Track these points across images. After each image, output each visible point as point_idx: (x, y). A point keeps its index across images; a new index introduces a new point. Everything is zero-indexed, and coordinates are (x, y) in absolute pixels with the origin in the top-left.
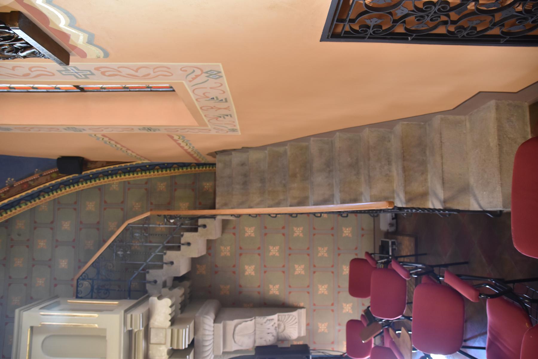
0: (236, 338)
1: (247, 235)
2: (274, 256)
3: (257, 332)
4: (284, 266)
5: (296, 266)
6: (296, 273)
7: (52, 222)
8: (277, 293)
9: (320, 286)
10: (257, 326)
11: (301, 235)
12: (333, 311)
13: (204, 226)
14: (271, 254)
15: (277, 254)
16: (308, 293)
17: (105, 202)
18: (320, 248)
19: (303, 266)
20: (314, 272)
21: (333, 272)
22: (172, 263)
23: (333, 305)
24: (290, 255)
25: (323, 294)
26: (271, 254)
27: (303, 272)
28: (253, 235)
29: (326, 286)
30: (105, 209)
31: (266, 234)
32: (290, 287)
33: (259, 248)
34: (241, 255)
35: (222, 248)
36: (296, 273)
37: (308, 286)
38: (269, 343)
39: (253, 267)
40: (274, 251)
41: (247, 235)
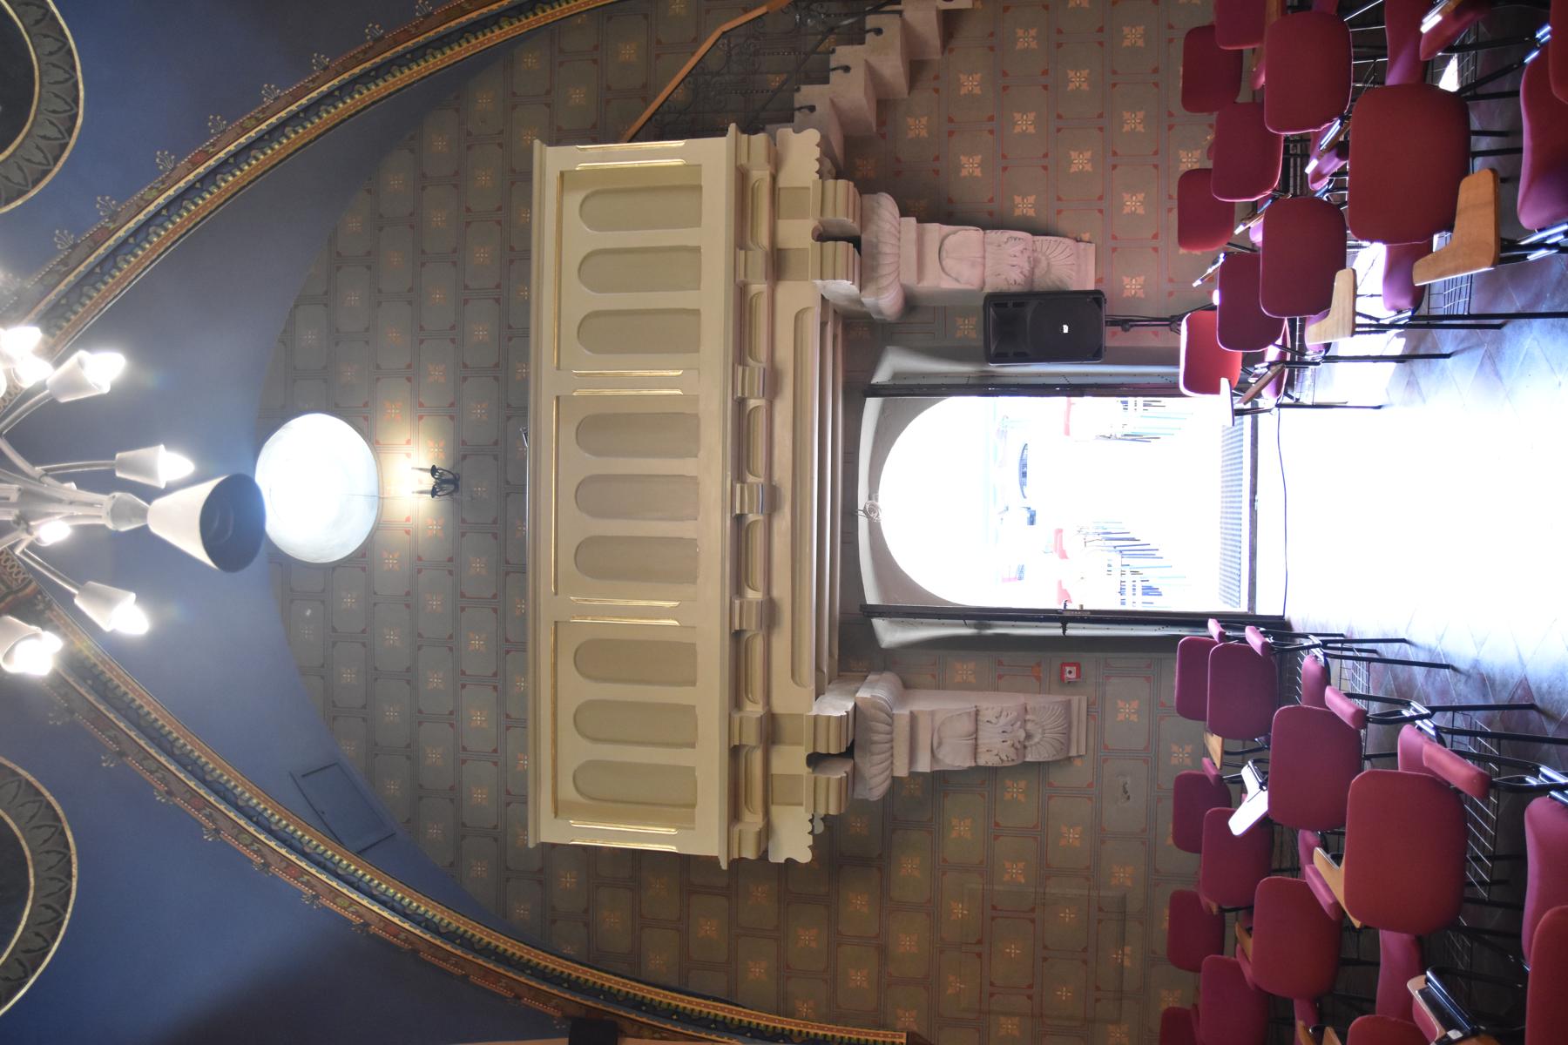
0: (948, 263)
1: (963, 91)
2: (1024, 134)
3: (989, 263)
4: (1046, 156)
5: (1074, 154)
6: (1074, 169)
7: (548, 92)
8: (1031, 213)
9: (1126, 197)
10: (989, 248)
11: (1085, 87)
12: (1155, 250)
13: (879, 31)
14: (1017, 130)
15: (1031, 130)
16: (1101, 211)
17: (659, 42)
18: (1126, 115)
19: (1088, 154)
20: (1114, 167)
21: (1156, 166)
22: (812, 109)
23: (1155, 236)
24: (1059, 130)
25: (1133, 213)
26: (1017, 130)
27: (1088, 168)
28: (977, 91)
29: (1141, 196)
30: (658, 56)
31: (1005, 88)
32: (1059, 199)
33: (991, 119)
34: (951, 133)
35: (910, 121)
36: (1074, 169)
37: (1101, 198)
38: (1014, 289)
39: (978, 158)
40: (1024, 123)
41: (963, 91)
